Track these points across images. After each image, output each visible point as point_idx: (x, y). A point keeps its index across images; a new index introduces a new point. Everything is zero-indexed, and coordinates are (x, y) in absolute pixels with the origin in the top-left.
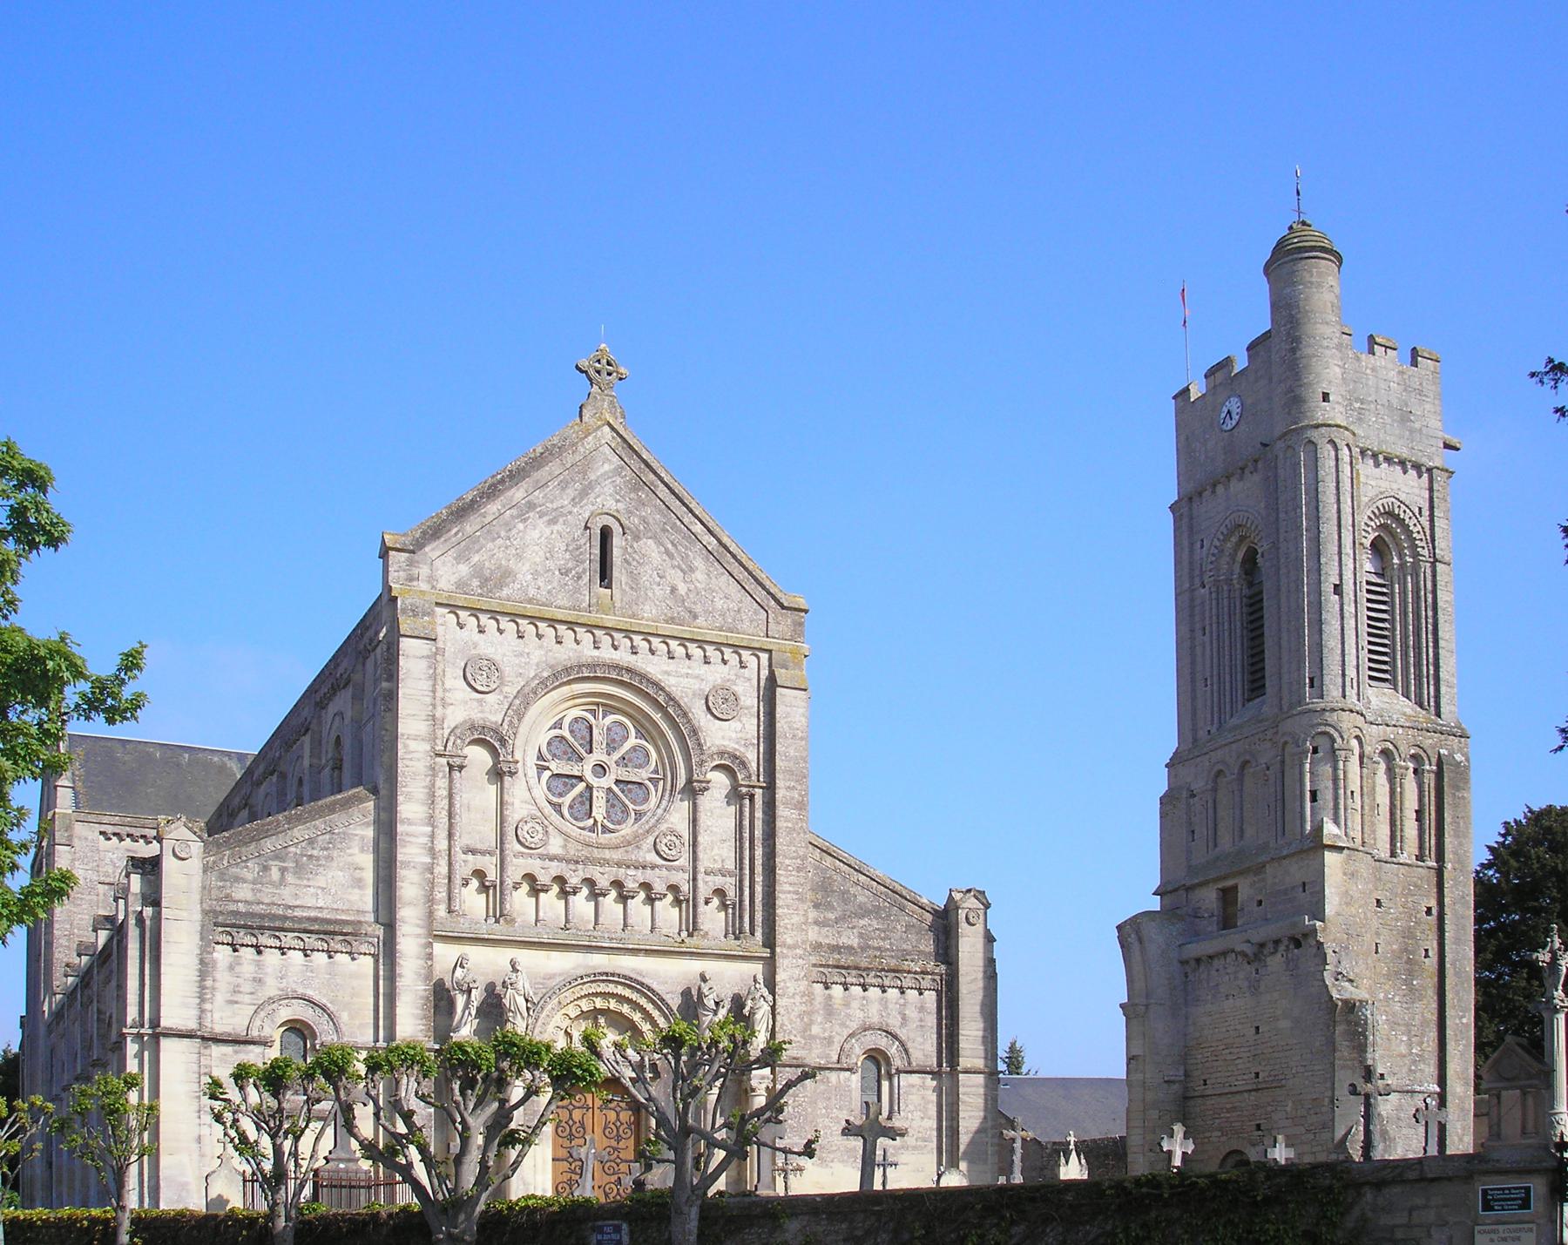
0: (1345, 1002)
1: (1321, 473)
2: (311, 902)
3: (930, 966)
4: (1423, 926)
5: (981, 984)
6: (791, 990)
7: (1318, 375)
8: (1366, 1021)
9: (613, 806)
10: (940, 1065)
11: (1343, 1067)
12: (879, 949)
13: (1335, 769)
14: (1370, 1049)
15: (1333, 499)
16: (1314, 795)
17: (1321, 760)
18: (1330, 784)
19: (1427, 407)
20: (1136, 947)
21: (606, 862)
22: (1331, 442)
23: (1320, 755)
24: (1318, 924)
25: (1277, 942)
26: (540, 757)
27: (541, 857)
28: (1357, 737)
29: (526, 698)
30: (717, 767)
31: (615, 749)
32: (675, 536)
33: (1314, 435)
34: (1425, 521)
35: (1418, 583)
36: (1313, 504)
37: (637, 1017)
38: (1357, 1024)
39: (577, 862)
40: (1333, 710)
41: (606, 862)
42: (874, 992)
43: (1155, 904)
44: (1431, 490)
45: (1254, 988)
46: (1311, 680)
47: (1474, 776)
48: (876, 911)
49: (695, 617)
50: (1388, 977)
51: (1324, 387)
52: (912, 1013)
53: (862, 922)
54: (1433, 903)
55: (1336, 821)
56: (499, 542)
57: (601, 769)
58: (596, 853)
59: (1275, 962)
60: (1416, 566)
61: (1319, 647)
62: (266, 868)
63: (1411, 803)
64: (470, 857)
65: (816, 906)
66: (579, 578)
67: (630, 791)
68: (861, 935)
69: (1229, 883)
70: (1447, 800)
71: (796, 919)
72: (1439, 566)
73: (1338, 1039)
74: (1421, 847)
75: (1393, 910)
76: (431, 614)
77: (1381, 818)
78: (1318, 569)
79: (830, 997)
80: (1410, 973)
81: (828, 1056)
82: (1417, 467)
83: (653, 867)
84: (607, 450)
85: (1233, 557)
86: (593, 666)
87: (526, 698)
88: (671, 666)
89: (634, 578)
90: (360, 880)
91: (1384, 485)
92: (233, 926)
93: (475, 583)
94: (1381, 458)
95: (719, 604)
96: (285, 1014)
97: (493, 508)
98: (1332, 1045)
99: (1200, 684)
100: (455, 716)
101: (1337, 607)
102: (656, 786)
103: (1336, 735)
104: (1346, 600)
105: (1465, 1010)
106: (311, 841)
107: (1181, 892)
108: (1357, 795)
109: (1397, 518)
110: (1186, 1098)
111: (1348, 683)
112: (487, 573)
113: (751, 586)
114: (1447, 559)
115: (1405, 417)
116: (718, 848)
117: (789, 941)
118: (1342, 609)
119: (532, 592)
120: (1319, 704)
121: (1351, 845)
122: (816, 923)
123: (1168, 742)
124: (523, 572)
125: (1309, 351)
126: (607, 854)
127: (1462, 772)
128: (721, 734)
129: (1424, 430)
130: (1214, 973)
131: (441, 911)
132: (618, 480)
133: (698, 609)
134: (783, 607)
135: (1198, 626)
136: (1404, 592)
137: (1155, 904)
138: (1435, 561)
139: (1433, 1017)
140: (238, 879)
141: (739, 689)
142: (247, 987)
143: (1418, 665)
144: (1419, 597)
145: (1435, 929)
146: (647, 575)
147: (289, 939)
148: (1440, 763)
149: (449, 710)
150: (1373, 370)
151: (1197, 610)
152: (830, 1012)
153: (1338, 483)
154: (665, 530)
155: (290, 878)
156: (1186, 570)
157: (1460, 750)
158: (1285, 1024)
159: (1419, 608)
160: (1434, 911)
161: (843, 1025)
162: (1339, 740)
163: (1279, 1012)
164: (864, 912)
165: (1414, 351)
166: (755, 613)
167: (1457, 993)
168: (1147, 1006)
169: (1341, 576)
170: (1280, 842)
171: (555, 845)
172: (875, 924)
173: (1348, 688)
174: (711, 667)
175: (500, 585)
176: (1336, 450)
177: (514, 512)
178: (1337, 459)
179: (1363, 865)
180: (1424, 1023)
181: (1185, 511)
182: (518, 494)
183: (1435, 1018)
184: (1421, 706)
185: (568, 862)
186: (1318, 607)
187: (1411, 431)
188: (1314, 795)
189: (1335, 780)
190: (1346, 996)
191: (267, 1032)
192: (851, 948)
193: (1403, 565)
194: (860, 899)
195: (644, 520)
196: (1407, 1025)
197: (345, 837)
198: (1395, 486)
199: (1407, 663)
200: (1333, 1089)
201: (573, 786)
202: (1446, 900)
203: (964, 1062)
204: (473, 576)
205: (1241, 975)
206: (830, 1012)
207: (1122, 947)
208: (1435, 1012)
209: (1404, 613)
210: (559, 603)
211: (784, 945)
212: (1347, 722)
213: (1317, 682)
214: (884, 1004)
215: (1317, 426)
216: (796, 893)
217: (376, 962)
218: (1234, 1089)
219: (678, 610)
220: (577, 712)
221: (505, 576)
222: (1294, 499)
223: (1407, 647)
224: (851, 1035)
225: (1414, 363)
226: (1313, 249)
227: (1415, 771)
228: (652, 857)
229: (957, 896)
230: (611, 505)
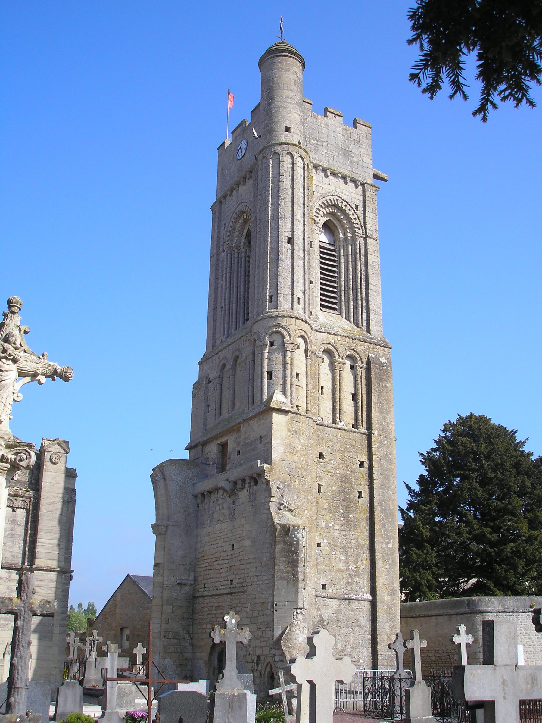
0: (283, 526)
1: (282, 171)
4: (357, 475)
5: (59, 505)
7: (283, 117)
8: (298, 544)
10: (23, 563)
11: (281, 579)
13: (285, 357)
14: (301, 565)
15: (289, 186)
16: (270, 373)
17: (275, 350)
18: (281, 367)
19: (362, 150)
20: (161, 483)
22: (289, 153)
23: (274, 347)
24: (266, 466)
25: (243, 480)
28: (302, 337)
33: (278, 149)
34: (360, 213)
35: (355, 249)
36: (277, 188)
38: (291, 544)
40: (283, 317)
43: (186, 455)
44: (364, 196)
45: (232, 518)
46: (271, 297)
47: (395, 372)
50: (329, 510)
54: (365, 458)
55: (284, 393)
59: (243, 495)
60: (354, 240)
61: (276, 276)
63: (348, 387)
69: (223, 440)
70: (374, 387)
72: (369, 240)
73: (277, 555)
74: (356, 419)
75: (333, 460)
77: (325, 396)
78: (277, 228)
80: (347, 509)
82: (354, 181)
85: (241, 233)
91: (331, 189)
94: (329, 172)
98: (272, 558)
99: (219, 311)
101: (290, 252)
103: (285, 333)
104: (296, 247)
105: (390, 538)
107: (200, 447)
108: (302, 377)
109: (340, 209)
110: (195, 597)
111: (295, 300)
114: (374, 237)
115: (347, 153)
118: (292, 253)
120: (275, 313)
121: (295, 410)
123: (200, 349)
125: (278, 104)
127: (385, 371)
129: (360, 163)
130: (211, 504)
135: (220, 276)
136: (346, 255)
137: (186, 455)
138: (365, 239)
139: (366, 542)
143: (355, 300)
144: (356, 258)
145: (366, 477)
148: (369, 363)
150: (326, 125)
151: (220, 265)
153: (293, 177)
156: (216, 242)
157: (384, 356)
158: (247, 543)
159: (356, 265)
162: (287, 337)
163: (245, 534)
165: (355, 120)
167: (384, 525)
168: (167, 526)
169: (293, 232)
170: (250, 409)
173: (296, 303)
176: (293, 158)
178: (293, 164)
179: (306, 426)
180: (359, 546)
181: (217, 208)
183: (367, 543)
184: (357, 326)
186: (276, 251)
187: (351, 162)
188: (270, 373)
189: (285, 364)
190: (284, 522)
193: (346, 239)
196: (345, 547)
198: (339, 190)
199: (349, 298)
200: (273, 596)
202: (374, 457)
203: (39, 562)
205: (225, 506)
207: (153, 483)
208: (368, 538)
209: (347, 268)
212: (293, 325)
213: (274, 299)
215: (281, 144)
217: (28, 513)
218: (218, 592)
222: (265, 187)
223: (349, 288)
225: (355, 127)
226: (284, 51)
227: (352, 367)
229: (46, 443)
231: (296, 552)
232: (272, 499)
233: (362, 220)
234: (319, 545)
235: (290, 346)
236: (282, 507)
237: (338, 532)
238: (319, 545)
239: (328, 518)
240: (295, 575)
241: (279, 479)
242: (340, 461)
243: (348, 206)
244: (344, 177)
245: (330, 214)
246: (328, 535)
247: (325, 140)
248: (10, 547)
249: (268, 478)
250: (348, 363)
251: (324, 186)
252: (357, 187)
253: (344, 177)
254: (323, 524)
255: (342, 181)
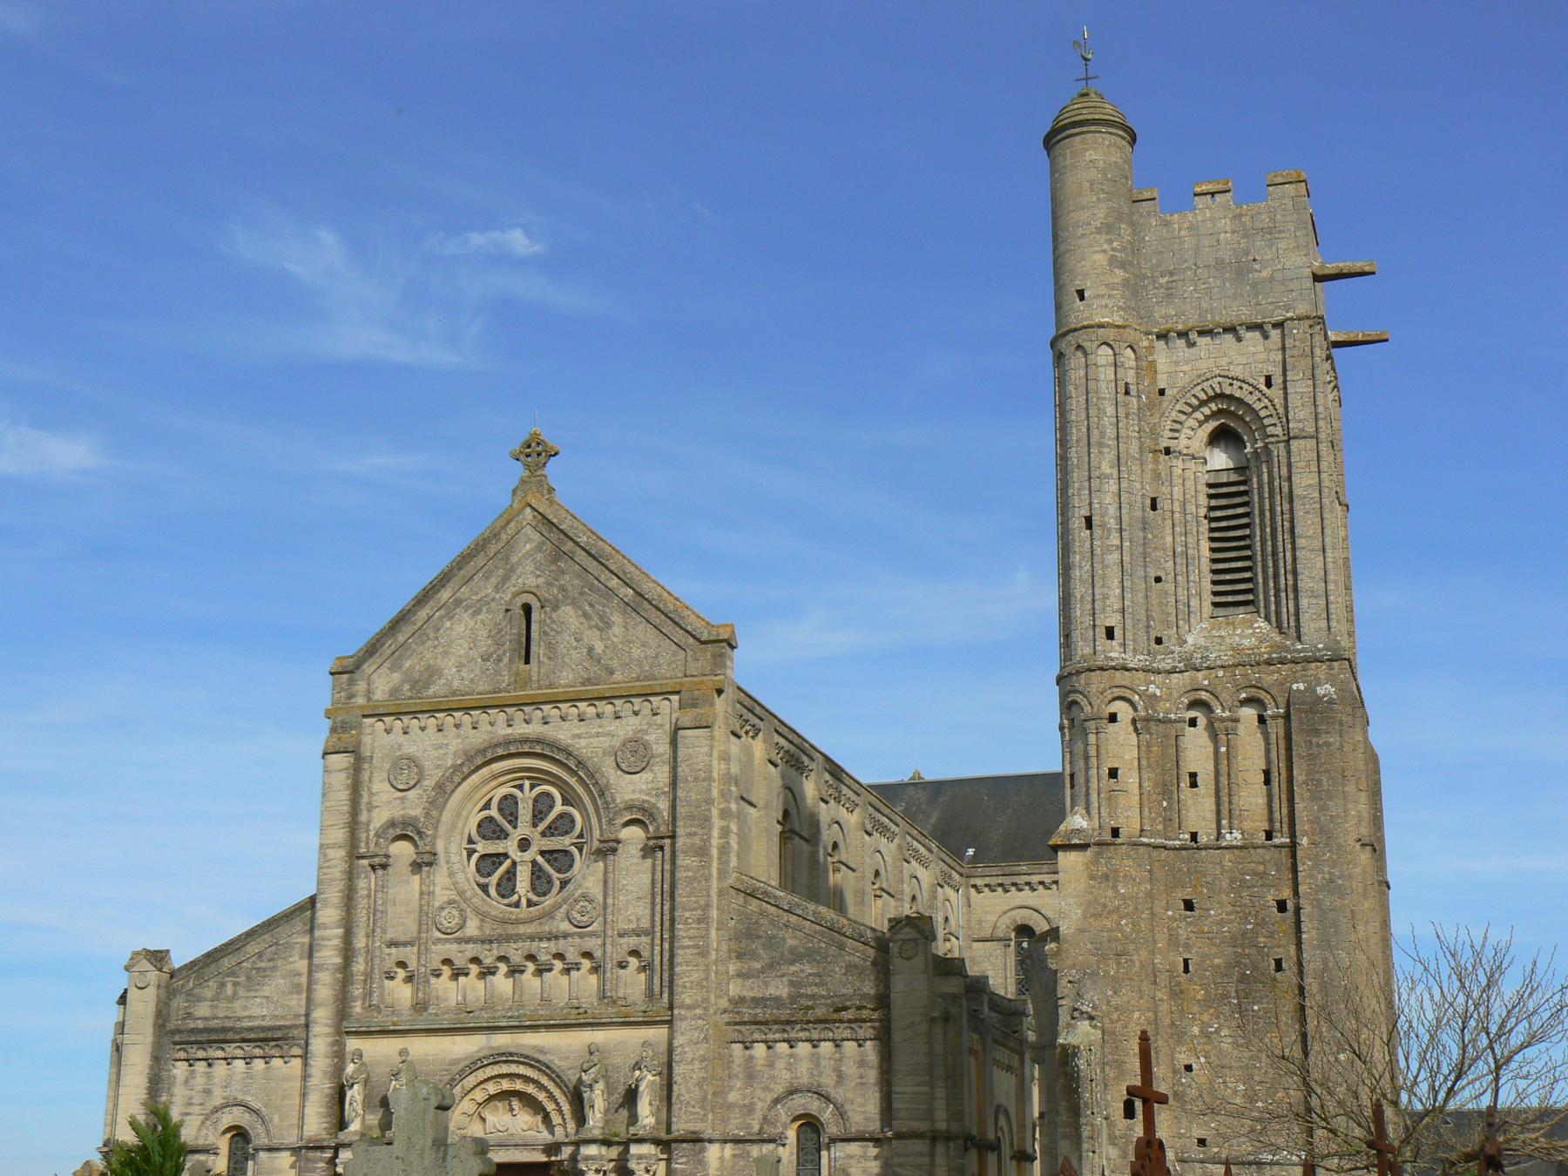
2: (257, 1012)
3: (865, 1014)
6: (689, 1056)
9: (539, 877)
12: (813, 997)
21: (517, 938)
22: (1079, 347)
26: (470, 841)
27: (459, 941)
29: (443, 791)
30: (627, 824)
31: (502, 830)
32: (593, 597)
34: (1276, 393)
37: (541, 1096)
39: (491, 942)
40: (1078, 673)
41: (517, 938)
42: (803, 1049)
48: (808, 955)
49: (612, 673)
50: (1207, 1002)
51: (1078, 284)
52: (850, 1069)
53: (793, 968)
54: (1286, 893)
56: (429, 643)
57: (524, 844)
58: (511, 930)
62: (223, 985)
64: (393, 950)
65: (740, 956)
66: (500, 660)
67: (556, 860)
68: (792, 984)
71: (696, 976)
76: (359, 726)
79: (751, 1058)
81: (749, 1126)
83: (565, 936)
84: (528, 530)
86: (508, 742)
87: (443, 791)
88: (581, 729)
89: (551, 647)
90: (299, 985)
91: (1203, 366)
92: (187, 1043)
93: (406, 687)
95: (637, 652)
96: (227, 1120)
97: (423, 614)
100: (379, 818)
102: (581, 850)
106: (260, 955)
112: (416, 675)
113: (668, 627)
116: (633, 908)
117: (688, 1001)
119: (456, 684)
122: (739, 975)
124: (450, 670)
126: (522, 929)
128: (631, 788)
129: (1279, 276)
131: (357, 1008)
132: (539, 556)
133: (615, 664)
134: (702, 643)
140: (199, 999)
141: (651, 738)
142: (197, 1100)
146: (565, 641)
147: (231, 1049)
149: (375, 814)
152: (750, 1076)
154: (582, 594)
155: (241, 992)
160: (1290, 905)
161: (767, 1089)
164: (797, 957)
166: (674, 655)
171: (472, 928)
172: (808, 969)
174: (623, 721)
175: (427, 686)
177: (442, 612)
182: (445, 595)
185: (483, 942)
191: (211, 1139)
192: (777, 999)
194: (791, 942)
195: (562, 589)
197: (289, 947)
201: (501, 864)
204: (404, 681)
206: (750, 1076)
210: (481, 688)
211: (682, 1006)
214: (815, 1060)
216: (697, 947)
219: (595, 669)
220: (505, 790)
221: (432, 673)
224: (776, 1101)
228: (565, 926)
230: (531, 581)
231: (1076, 1091)
232: (1061, 1002)
233: (1281, 411)
234: (1189, 1068)
235: (1091, 725)
236: (1076, 1014)
237: (1230, 1040)
238: (1189, 1068)
239: (1206, 1017)
240: (1077, 1128)
241: (1074, 966)
242: (1230, 908)
243: (1245, 386)
244: (1231, 329)
245: (1215, 415)
246: (1207, 1048)
247: (1190, 264)
248: (861, 1105)
249: (1054, 967)
250: (1249, 713)
251: (1185, 368)
252: (1266, 337)
253: (1231, 329)
254: (1196, 1030)
255: (1229, 337)
